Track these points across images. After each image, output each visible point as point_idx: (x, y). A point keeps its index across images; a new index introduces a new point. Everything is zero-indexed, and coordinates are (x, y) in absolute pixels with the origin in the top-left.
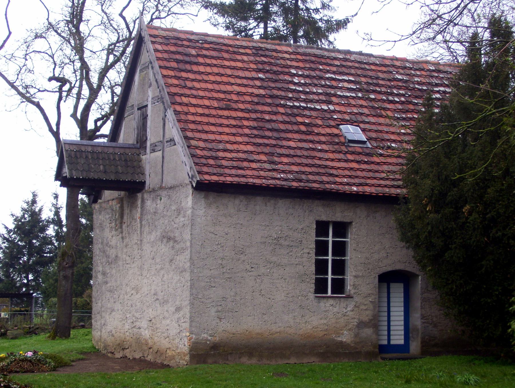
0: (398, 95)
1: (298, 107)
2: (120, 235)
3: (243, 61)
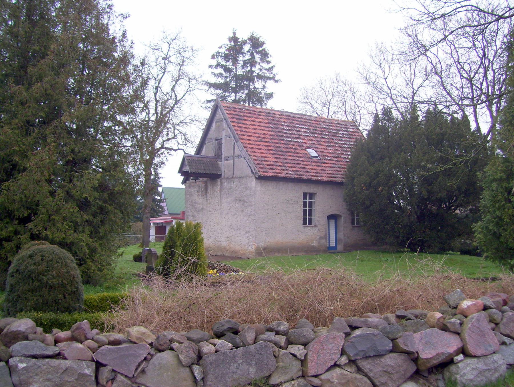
0: (326, 135)
1: (288, 141)
2: (205, 198)
3: (262, 119)
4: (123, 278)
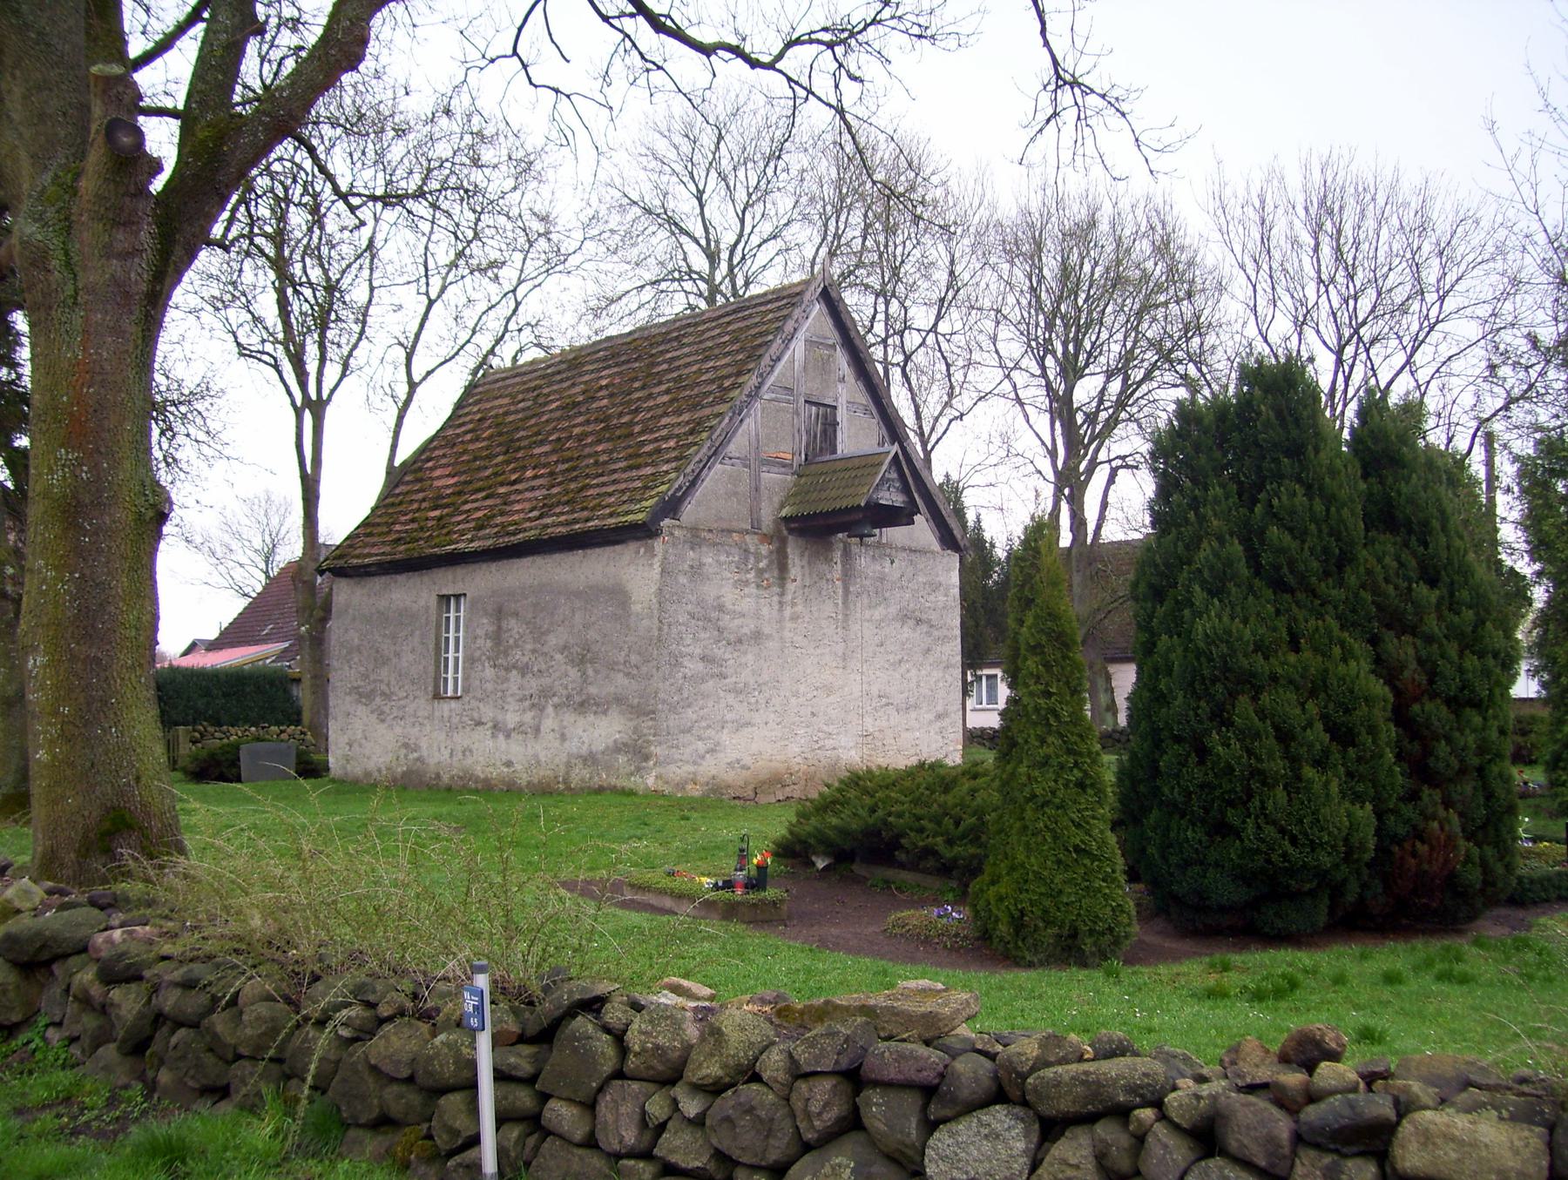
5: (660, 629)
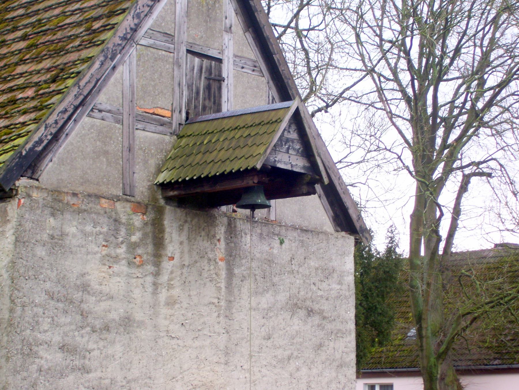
4: (292, 354)
5: (11, 311)
